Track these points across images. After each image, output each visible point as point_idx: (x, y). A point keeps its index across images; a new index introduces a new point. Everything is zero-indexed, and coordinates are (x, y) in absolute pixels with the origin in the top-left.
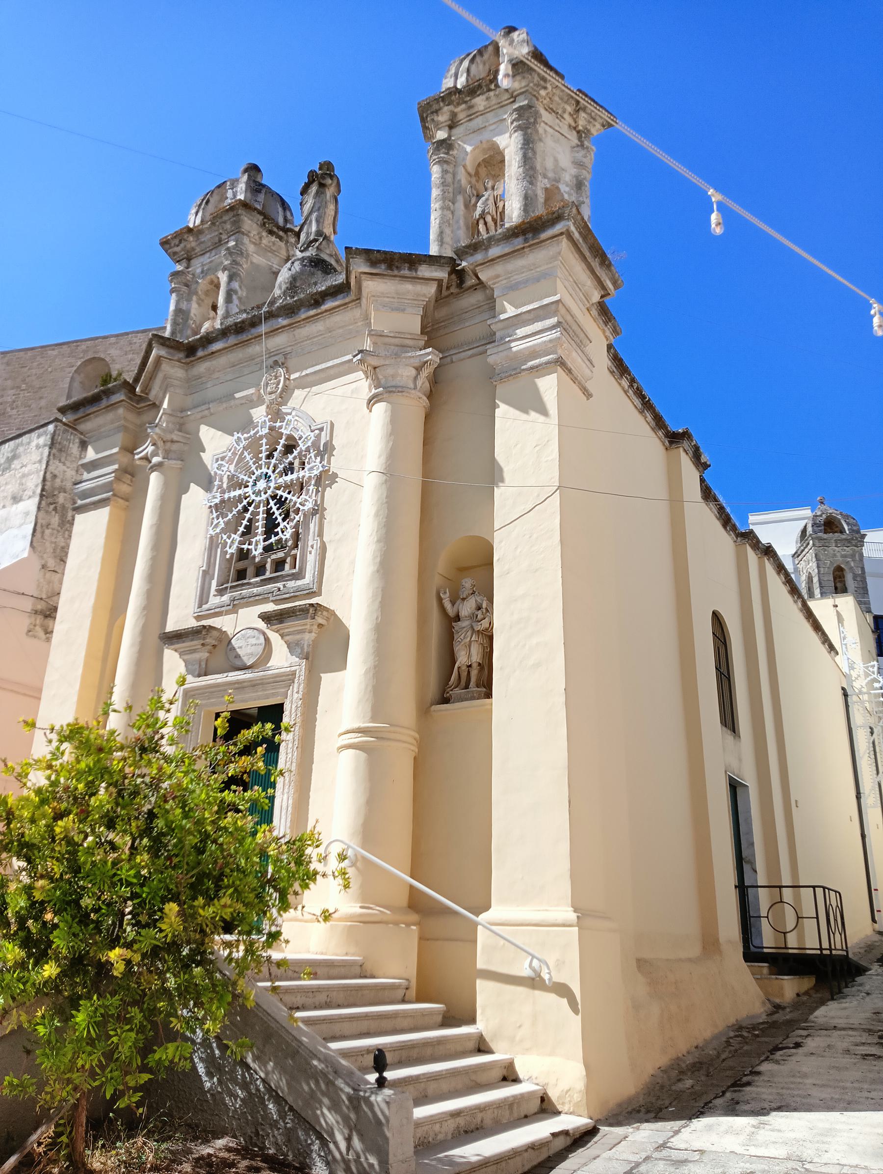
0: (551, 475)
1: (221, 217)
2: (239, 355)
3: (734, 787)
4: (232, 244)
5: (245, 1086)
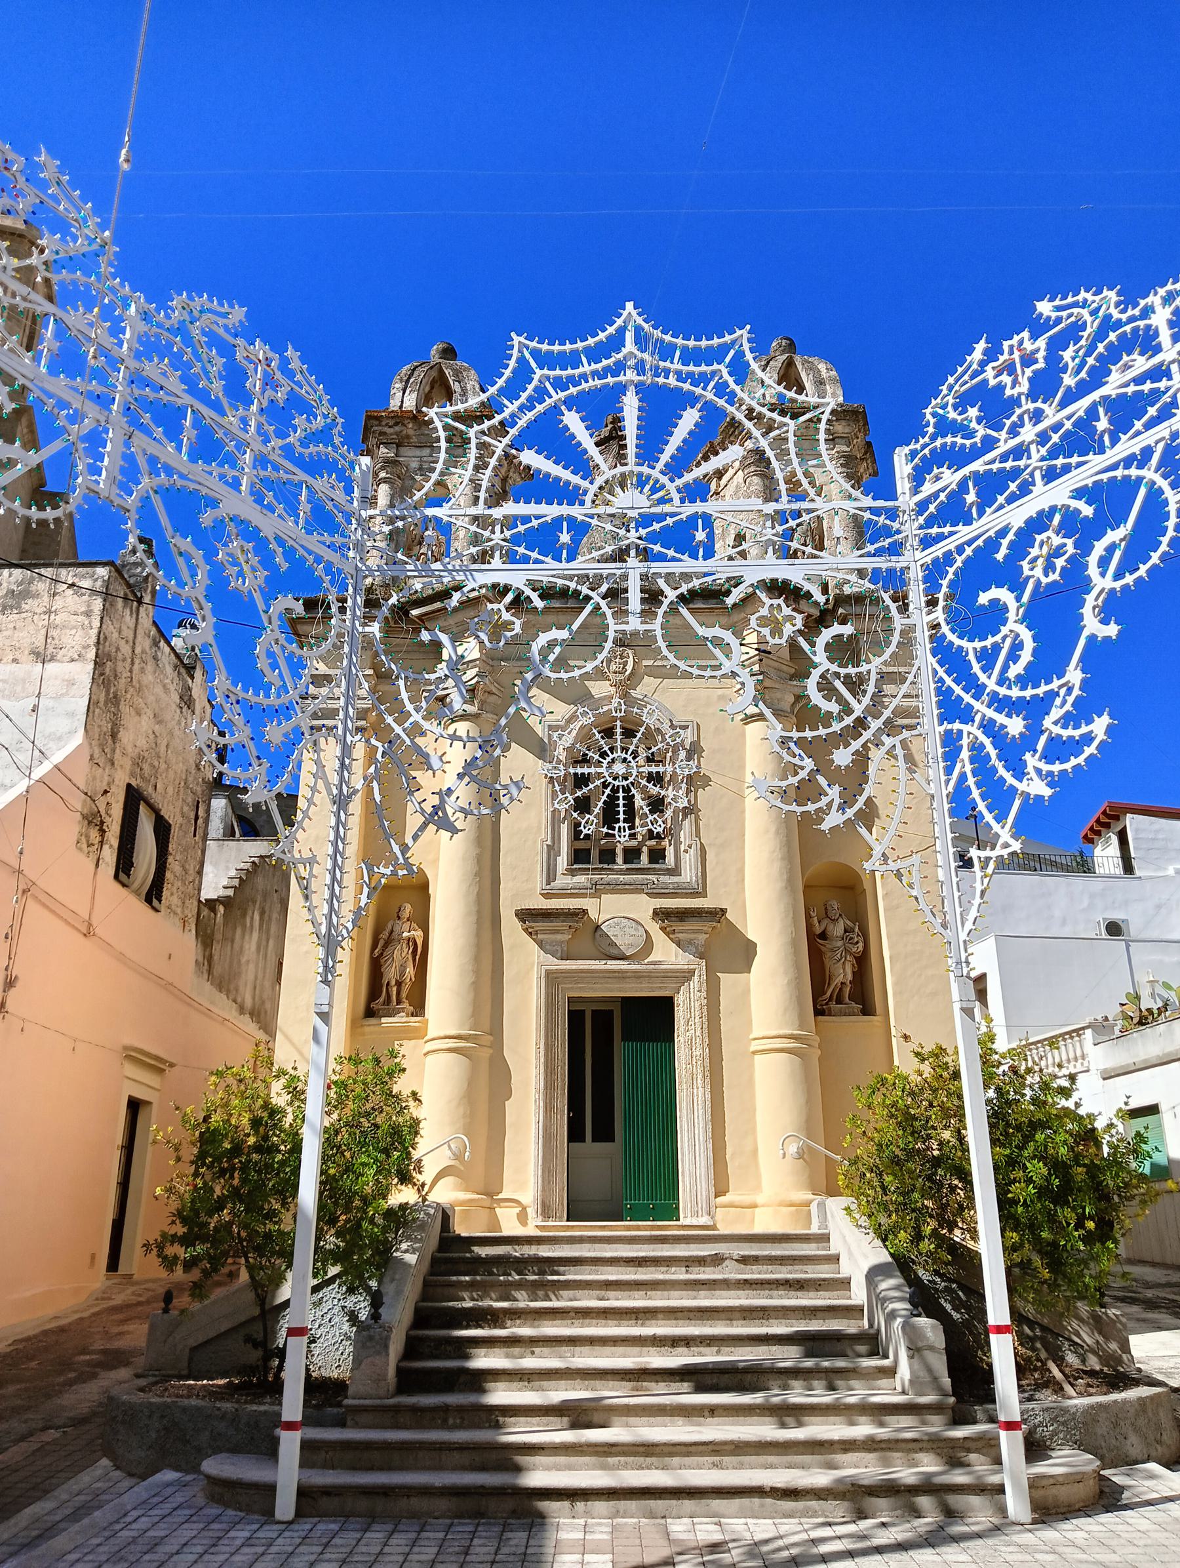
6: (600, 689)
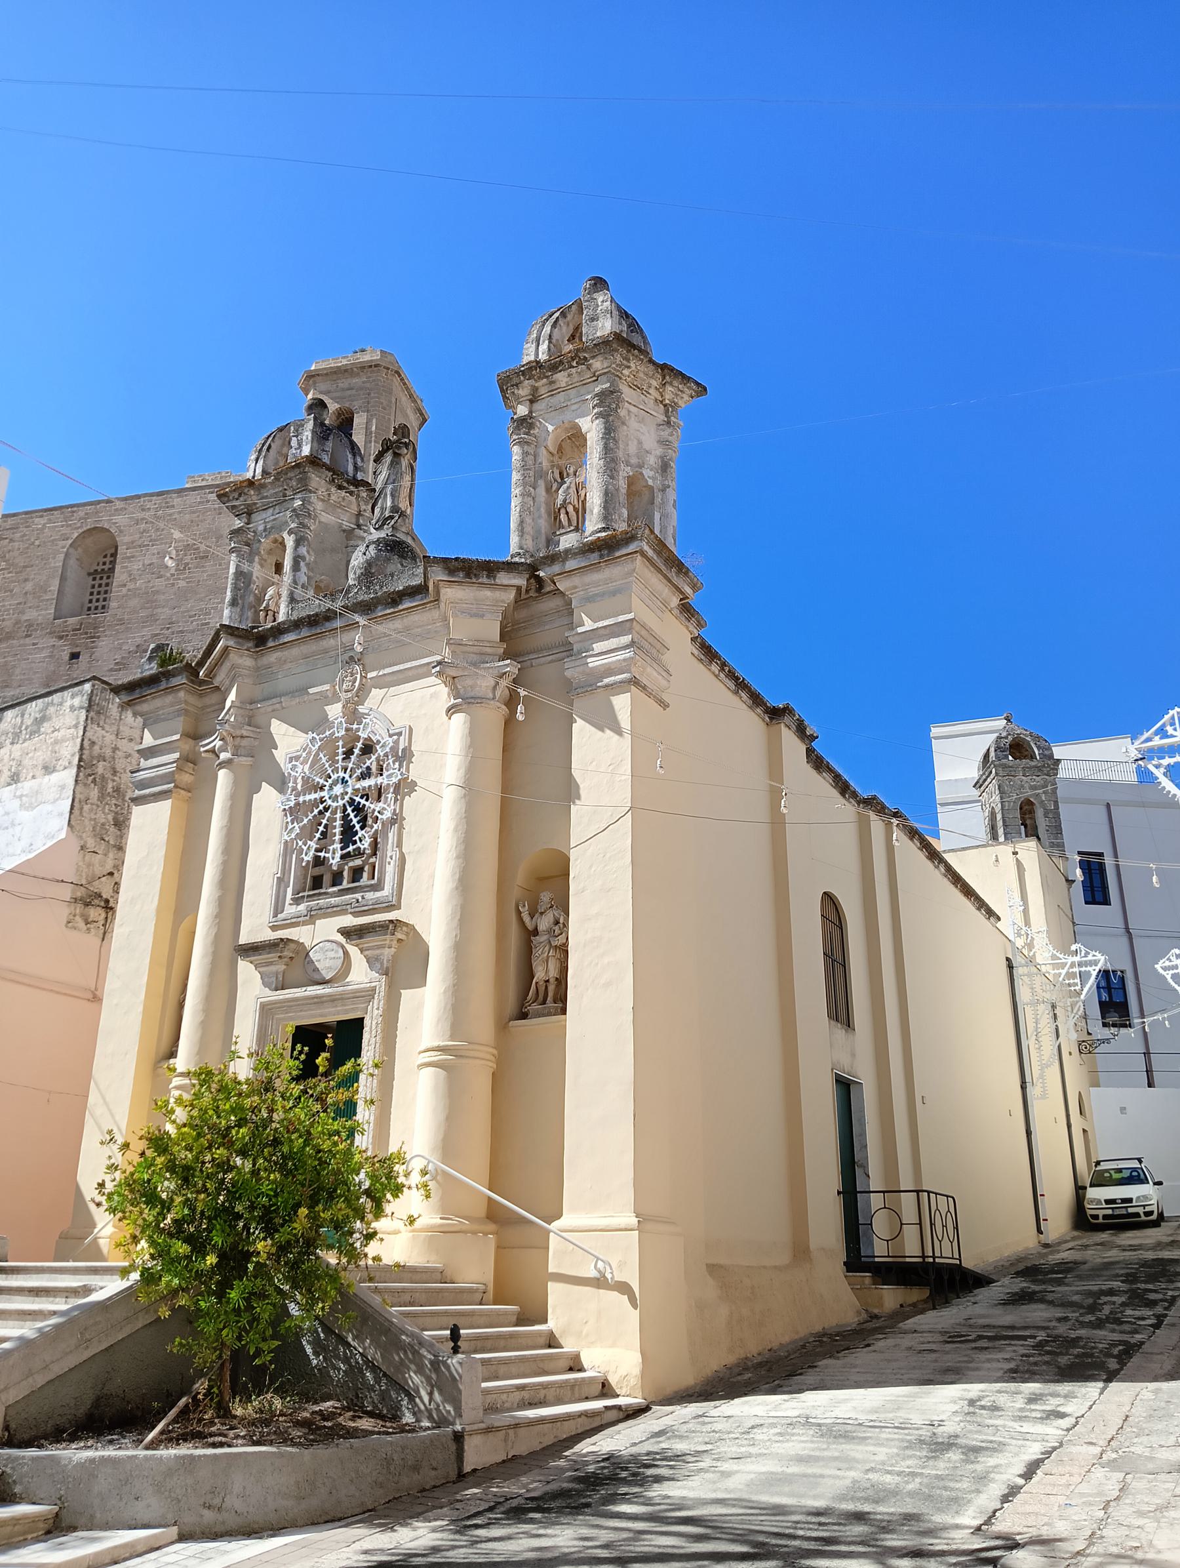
0: (624, 796)
2: (312, 647)
3: (845, 1087)
4: (298, 503)
5: (346, 1360)
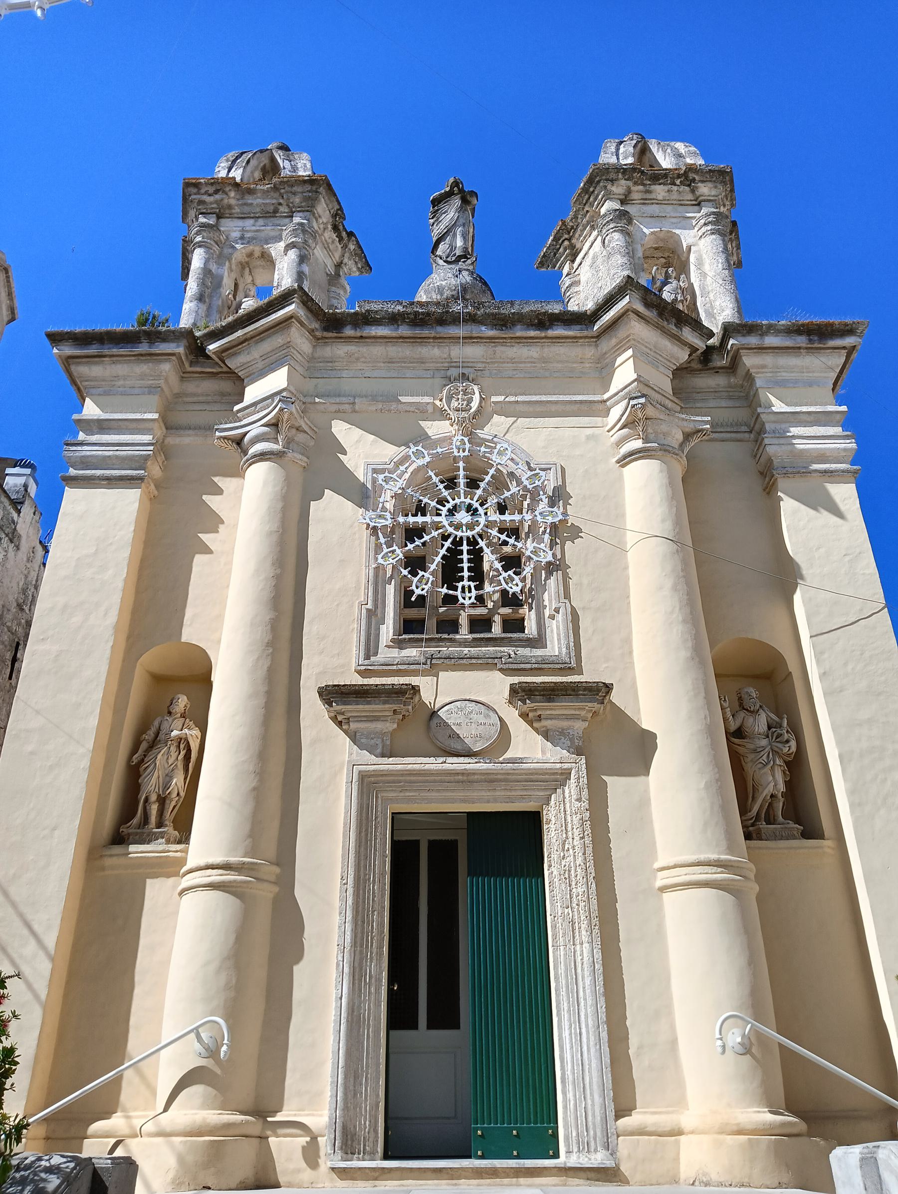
1: (292, 186)
6: (436, 429)
